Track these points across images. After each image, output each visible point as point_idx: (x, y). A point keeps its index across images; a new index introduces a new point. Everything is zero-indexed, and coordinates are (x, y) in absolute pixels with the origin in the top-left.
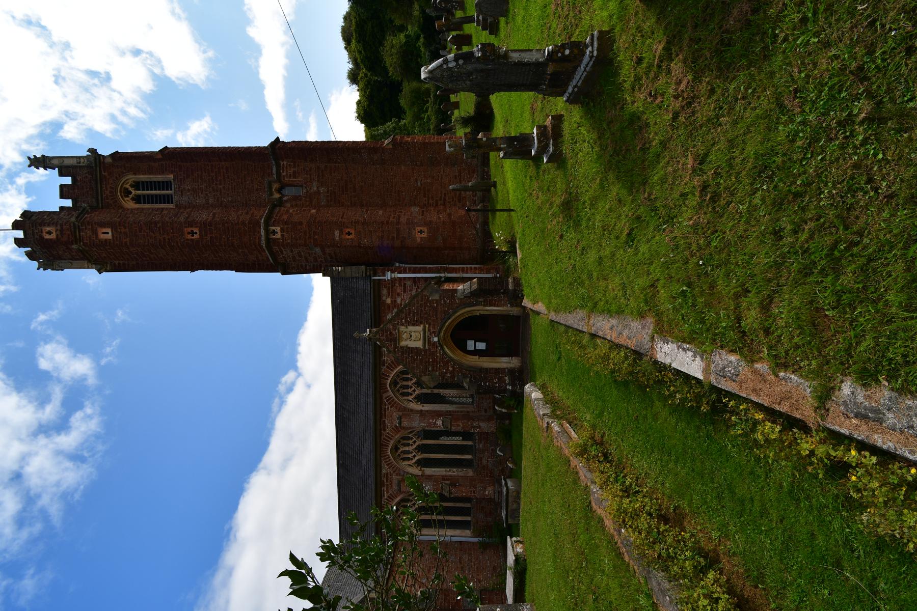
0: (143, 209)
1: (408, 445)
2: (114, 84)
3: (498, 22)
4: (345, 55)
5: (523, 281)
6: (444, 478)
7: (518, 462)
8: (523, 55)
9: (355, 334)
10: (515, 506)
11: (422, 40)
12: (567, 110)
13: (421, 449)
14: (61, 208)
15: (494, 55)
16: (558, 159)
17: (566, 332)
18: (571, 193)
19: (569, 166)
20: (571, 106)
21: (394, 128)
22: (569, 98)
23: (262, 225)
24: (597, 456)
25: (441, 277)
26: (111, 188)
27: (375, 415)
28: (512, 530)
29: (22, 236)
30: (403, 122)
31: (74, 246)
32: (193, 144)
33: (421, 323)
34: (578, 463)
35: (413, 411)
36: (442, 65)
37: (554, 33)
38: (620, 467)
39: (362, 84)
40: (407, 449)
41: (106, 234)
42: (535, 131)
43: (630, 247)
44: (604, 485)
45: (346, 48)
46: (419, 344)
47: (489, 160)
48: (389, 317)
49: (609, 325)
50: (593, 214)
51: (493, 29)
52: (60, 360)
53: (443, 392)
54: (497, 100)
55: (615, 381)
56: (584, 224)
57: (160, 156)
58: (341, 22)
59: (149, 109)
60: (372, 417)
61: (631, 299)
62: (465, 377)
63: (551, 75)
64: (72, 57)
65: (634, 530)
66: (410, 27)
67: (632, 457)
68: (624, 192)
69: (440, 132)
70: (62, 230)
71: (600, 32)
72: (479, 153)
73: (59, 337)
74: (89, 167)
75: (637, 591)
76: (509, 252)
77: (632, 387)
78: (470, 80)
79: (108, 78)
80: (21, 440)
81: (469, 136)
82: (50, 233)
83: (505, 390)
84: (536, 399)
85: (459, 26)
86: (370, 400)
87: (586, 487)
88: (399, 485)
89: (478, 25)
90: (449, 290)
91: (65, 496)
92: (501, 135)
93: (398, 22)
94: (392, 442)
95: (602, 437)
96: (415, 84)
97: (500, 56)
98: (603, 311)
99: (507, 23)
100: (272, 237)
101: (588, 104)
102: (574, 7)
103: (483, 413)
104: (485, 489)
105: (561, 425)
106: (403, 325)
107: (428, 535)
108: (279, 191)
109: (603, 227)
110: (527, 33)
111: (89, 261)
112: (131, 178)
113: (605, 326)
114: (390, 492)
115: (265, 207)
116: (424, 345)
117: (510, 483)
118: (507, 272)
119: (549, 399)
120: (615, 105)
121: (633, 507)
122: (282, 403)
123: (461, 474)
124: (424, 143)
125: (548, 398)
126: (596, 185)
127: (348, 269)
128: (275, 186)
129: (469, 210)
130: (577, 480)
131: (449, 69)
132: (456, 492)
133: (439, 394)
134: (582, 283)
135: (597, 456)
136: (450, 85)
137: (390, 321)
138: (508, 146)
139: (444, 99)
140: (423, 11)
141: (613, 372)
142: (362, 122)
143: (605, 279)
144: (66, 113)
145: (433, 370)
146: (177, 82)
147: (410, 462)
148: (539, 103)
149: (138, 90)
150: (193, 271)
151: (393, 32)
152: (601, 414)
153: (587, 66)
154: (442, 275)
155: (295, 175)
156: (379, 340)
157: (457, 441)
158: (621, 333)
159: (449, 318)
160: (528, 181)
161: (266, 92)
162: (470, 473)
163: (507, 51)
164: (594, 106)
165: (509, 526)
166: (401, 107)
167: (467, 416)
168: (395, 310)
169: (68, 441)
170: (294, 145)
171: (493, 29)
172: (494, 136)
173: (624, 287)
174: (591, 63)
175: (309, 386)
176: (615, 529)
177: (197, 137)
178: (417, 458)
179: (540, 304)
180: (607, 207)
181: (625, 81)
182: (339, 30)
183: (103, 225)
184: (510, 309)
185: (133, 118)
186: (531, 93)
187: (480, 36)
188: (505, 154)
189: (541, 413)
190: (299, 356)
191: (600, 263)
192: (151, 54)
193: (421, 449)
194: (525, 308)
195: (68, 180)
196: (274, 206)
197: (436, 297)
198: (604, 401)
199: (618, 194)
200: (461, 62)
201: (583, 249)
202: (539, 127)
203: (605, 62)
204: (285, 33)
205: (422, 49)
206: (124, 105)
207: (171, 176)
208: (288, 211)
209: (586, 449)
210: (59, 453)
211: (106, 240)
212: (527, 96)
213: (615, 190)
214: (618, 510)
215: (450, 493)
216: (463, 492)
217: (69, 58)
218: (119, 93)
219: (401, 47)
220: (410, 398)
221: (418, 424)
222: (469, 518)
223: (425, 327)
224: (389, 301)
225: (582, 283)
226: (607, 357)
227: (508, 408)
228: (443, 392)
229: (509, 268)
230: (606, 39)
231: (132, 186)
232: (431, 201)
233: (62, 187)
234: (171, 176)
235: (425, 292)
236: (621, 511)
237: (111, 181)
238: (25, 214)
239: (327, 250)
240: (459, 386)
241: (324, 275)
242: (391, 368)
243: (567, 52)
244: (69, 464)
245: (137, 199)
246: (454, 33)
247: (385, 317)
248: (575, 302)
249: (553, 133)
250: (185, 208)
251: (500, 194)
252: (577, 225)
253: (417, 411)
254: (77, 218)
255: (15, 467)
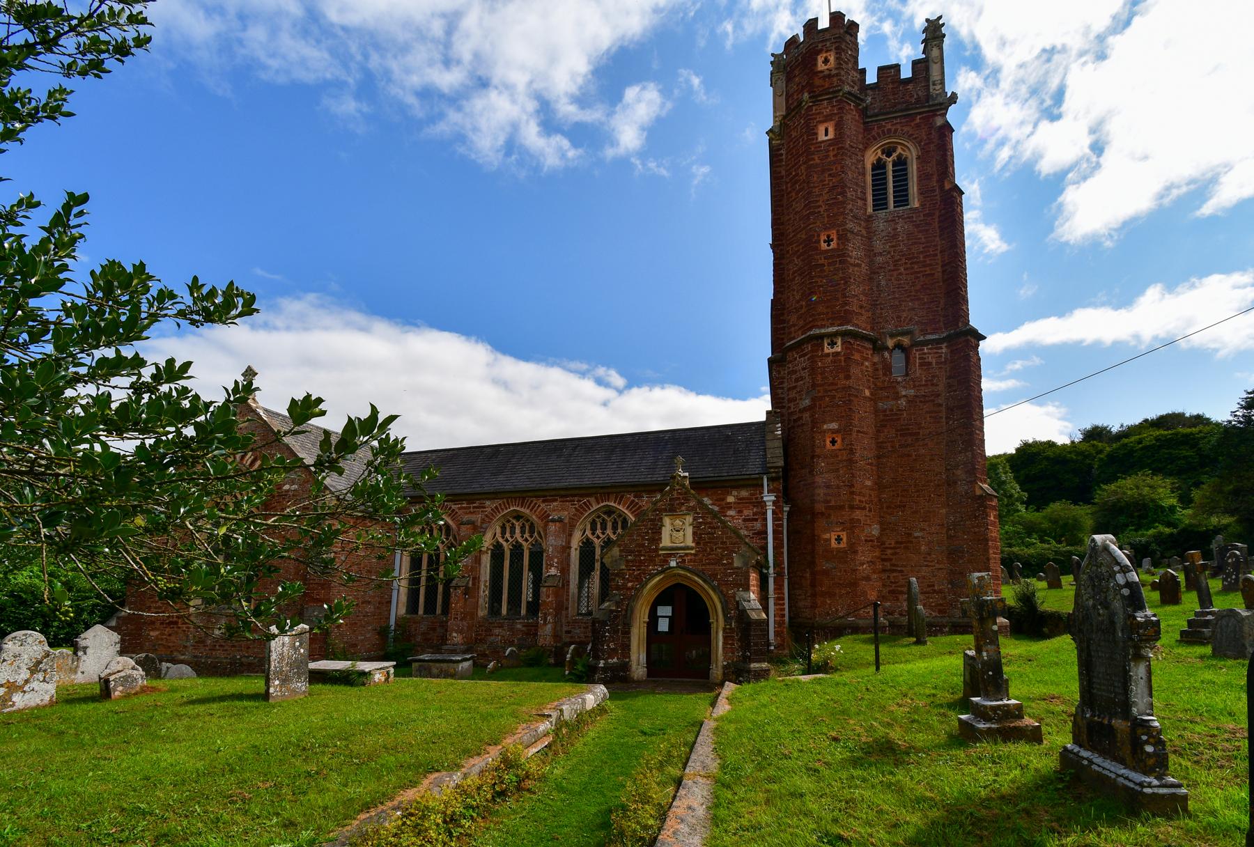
0: (864, 174)
1: (523, 532)
2: (1045, 126)
3: (1202, 644)
4: (1134, 418)
5: (763, 683)
6: (476, 580)
7: (494, 675)
8: (1142, 683)
9: (680, 458)
10: (435, 671)
11: (1167, 530)
12: (1051, 749)
13: (517, 550)
14: (863, 71)
15: (1141, 640)
16: (966, 735)
17: (685, 744)
18: (908, 754)
19: (954, 752)
20: (1056, 756)
21: (1011, 496)
22: (1071, 752)
23: (844, 328)
24: (502, 782)
25: (768, 568)
26: (896, 131)
27: (566, 489)
28: (403, 668)
29: (820, 27)
30: (1022, 508)
31: (806, 96)
32: (968, 229)
33: (698, 543)
34: (492, 756)
35: (568, 536)
36: (1118, 564)
37: (1185, 729)
38: (486, 813)
39: (1085, 447)
40: (518, 530)
41: (825, 133)
42: (1013, 702)
43: (820, 839)
44: (461, 790)
45: (1146, 421)
46: (666, 542)
47: (962, 633)
48: (707, 500)
49: (695, 805)
50: (873, 787)
51: (1191, 636)
52: (636, 114)
53: (596, 575)
54: (1064, 645)
55: (611, 811)
56: (857, 772)
57: (947, 186)
58: (1190, 410)
59: (1007, 174)
60: (562, 485)
61: (736, 838)
62: (618, 604)
63: (1110, 726)
64: (1085, 63)
65: (398, 828)
66: (1189, 511)
67: (499, 830)
68: (911, 832)
69: (1007, 562)
70: (829, 76)
71: (1185, 798)
72: (975, 620)
73: (669, 105)
74: (928, 97)
75: (319, 828)
76: (809, 664)
77: (602, 834)
78: (1094, 606)
79: (1054, 117)
80: (531, 82)
81: (999, 605)
82: (825, 63)
83: (597, 658)
84: (584, 700)
85: (1193, 584)
86: (586, 482)
87: (459, 766)
88: (468, 523)
89: (1197, 614)
90: (748, 579)
91: (461, 138)
92: (1003, 651)
93: (1196, 494)
94: (528, 511)
95: (529, 790)
96: (1089, 522)
97: (1137, 648)
98: (717, 797)
99: (1202, 657)
100: (826, 342)
101: (1061, 780)
102: (1229, 759)
103: (565, 629)
104: (460, 632)
105: (546, 735)
106: (694, 519)
107: (402, 562)
108: (899, 346)
109: (853, 800)
110: (1182, 689)
111: (784, 117)
112: (911, 153)
113: (695, 798)
114: (460, 512)
115: (872, 329)
116: (663, 549)
117: (466, 664)
118: (778, 661)
119: (583, 719)
120: (1059, 819)
121: (430, 828)
122: (583, 374)
123: (481, 601)
124: (987, 540)
125: (586, 717)
126: (921, 790)
127: (779, 444)
128: (906, 341)
129: (876, 606)
130: (468, 753)
131: (1112, 575)
132: (456, 595)
133: (593, 569)
134: (760, 768)
135: (502, 782)
136: (1085, 577)
137: (701, 503)
138: (984, 663)
139: (1067, 565)
140: (1217, 530)
141: (624, 808)
142: (1017, 450)
143: (767, 802)
144: (996, 71)
145: (627, 561)
146: (1054, 205)
147: (499, 536)
148: (1062, 707)
149: (1037, 157)
150: (773, 246)
151: (1179, 488)
152: (560, 789)
153: (1127, 778)
154: (771, 570)
155: (925, 364)
156: (672, 489)
157: (527, 594)
158: (682, 821)
159: (705, 581)
160: (927, 692)
161: (1053, 320)
162: (482, 613)
163: (1148, 659)
164: (1057, 790)
165: (409, 664)
166: (1047, 505)
167: (560, 607)
168: (716, 509)
169: (531, 135)
170: (974, 360)
171: (1191, 636)
172: (1001, 639)
173: (756, 827)
174: (1131, 785)
175: (605, 404)
176: (401, 802)
177: (975, 236)
178: (504, 544)
179: (728, 707)
180: (886, 807)
181: (1099, 835)
182: (1178, 410)
183: (839, 127)
184: (720, 664)
185: (992, 157)
186: (1077, 697)
187: (1174, 619)
188: (972, 658)
189: (564, 707)
190: (645, 389)
191: (792, 795)
192: (1098, 166)
193: (517, 549)
194: (722, 685)
195: (906, 73)
196: (873, 341)
197: (737, 563)
198: (580, 794)
199: (908, 823)
200: (1126, 592)
201: (816, 771)
202: (1019, 708)
203: (1131, 806)
204: (1155, 338)
205: (1151, 532)
206: (1014, 141)
207: (916, 205)
208: (867, 359)
209: (512, 767)
210: (515, 126)
211: (816, 134)
212: (1072, 690)
213: (914, 820)
214: (427, 808)
215: (456, 588)
216: (457, 604)
217: (1084, 59)
218: (1032, 133)
219: (1153, 500)
220: (588, 533)
221: (552, 543)
222: (421, 612)
223: (692, 548)
224: (731, 499)
225: (760, 768)
226: (645, 800)
227: (573, 662)
228: (596, 575)
229: (784, 663)
230: (1173, 806)
231: (899, 156)
232: (889, 552)
233: (897, 67)
234: (916, 205)
235: (744, 548)
236: (425, 812)
237: (906, 129)
238: (854, 26)
239: (806, 415)
240: (604, 596)
241: (768, 413)
242: (632, 506)
243: (1149, 749)
244: (501, 140)
245: (879, 166)
246: (1181, 578)
247: (707, 496)
248: (731, 757)
249: (1009, 727)
250: (867, 228)
251: (905, 650)
252: (855, 763)
253: (569, 542)
254: (849, 93)
255: (495, 81)
